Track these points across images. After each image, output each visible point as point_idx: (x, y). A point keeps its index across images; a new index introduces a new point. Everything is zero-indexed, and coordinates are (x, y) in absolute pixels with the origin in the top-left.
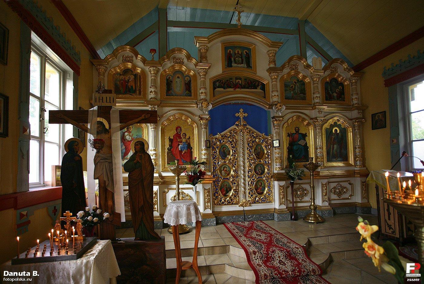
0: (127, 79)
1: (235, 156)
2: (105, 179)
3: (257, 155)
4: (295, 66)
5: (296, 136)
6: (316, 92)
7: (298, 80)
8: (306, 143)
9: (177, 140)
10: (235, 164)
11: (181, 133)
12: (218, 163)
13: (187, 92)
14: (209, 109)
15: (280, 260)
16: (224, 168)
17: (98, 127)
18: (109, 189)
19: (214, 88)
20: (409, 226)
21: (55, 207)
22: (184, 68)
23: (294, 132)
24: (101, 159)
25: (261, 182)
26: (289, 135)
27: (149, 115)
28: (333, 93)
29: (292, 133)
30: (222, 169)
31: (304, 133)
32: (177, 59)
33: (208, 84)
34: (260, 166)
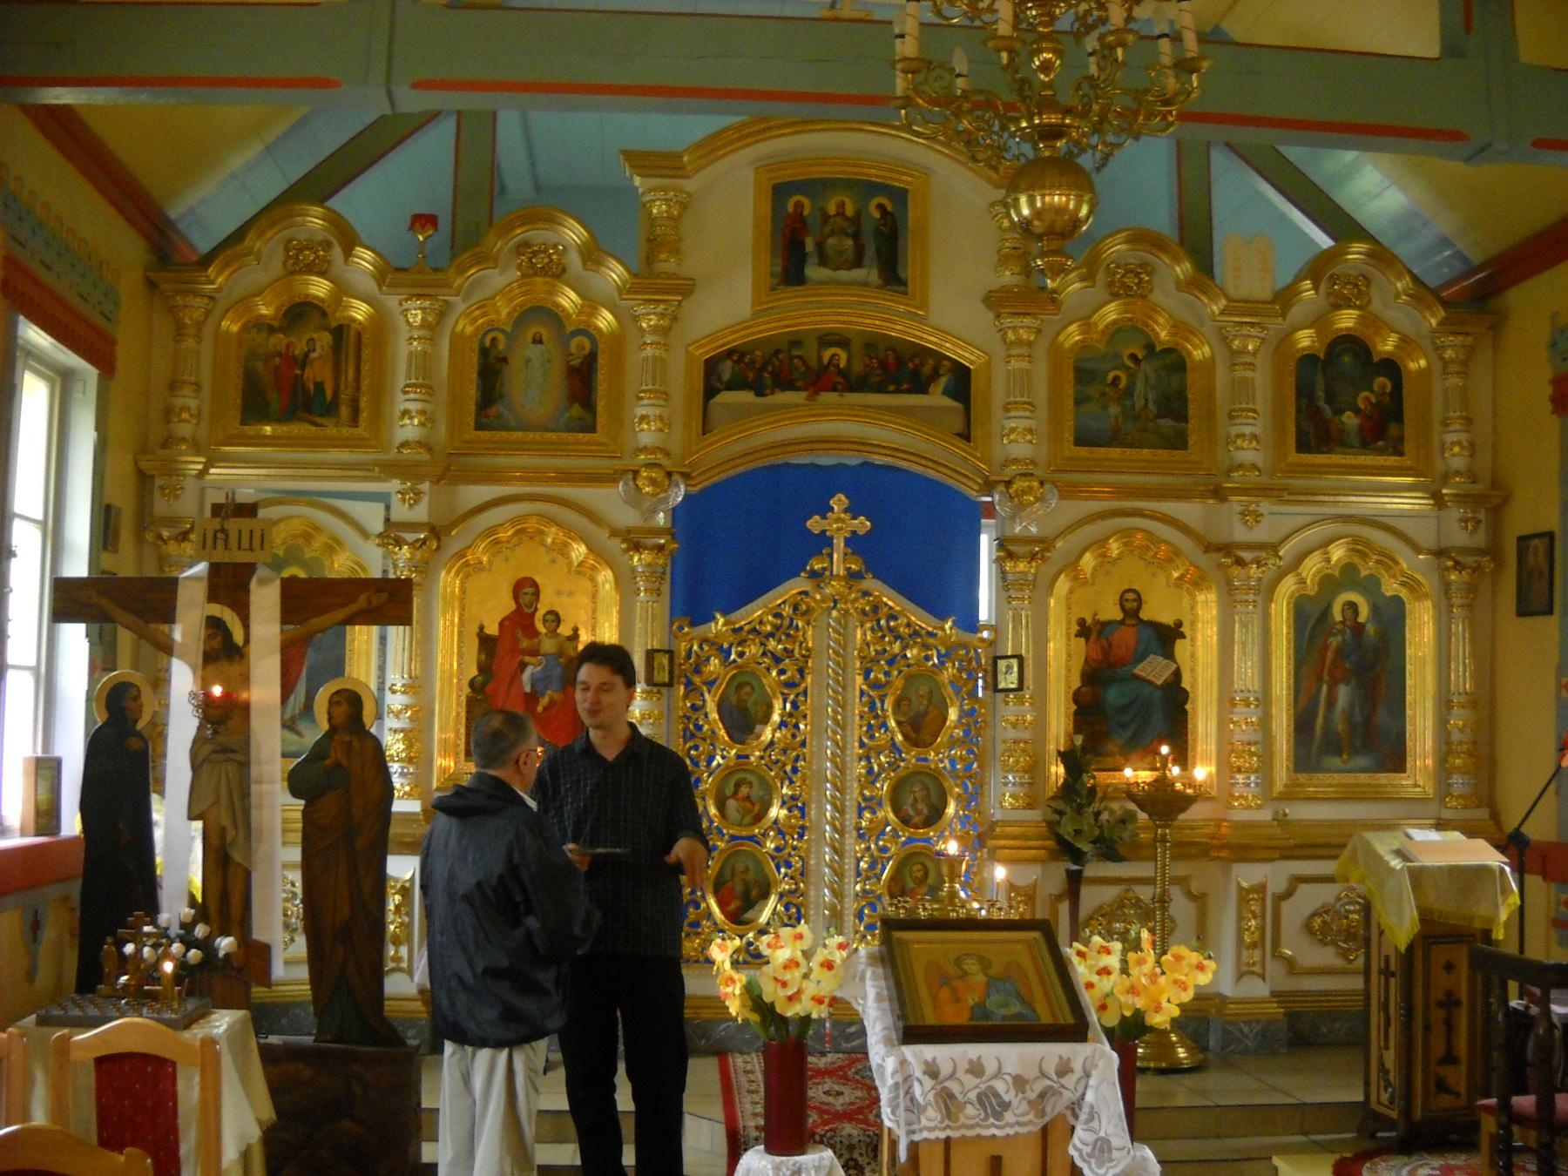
0: (299, 349)
1: (796, 726)
2: (226, 821)
3: (908, 729)
4: (1137, 275)
5: (1126, 638)
6: (1243, 410)
7: (1150, 347)
8: (1177, 674)
9: (516, 642)
10: (795, 770)
11: (536, 609)
12: (711, 758)
13: (576, 410)
14: (671, 504)
15: (851, 1159)
16: (738, 785)
17: (209, 638)
18: (237, 855)
19: (710, 392)
20: (1444, 1071)
21: (36, 912)
22: (568, 299)
23: (1112, 612)
24: (215, 752)
25: (922, 864)
26: (1084, 630)
27: (385, 596)
28: (1338, 412)
29: (1103, 617)
30: (729, 790)
31: (1167, 618)
32: (535, 254)
33: (683, 379)
34: (923, 783)
